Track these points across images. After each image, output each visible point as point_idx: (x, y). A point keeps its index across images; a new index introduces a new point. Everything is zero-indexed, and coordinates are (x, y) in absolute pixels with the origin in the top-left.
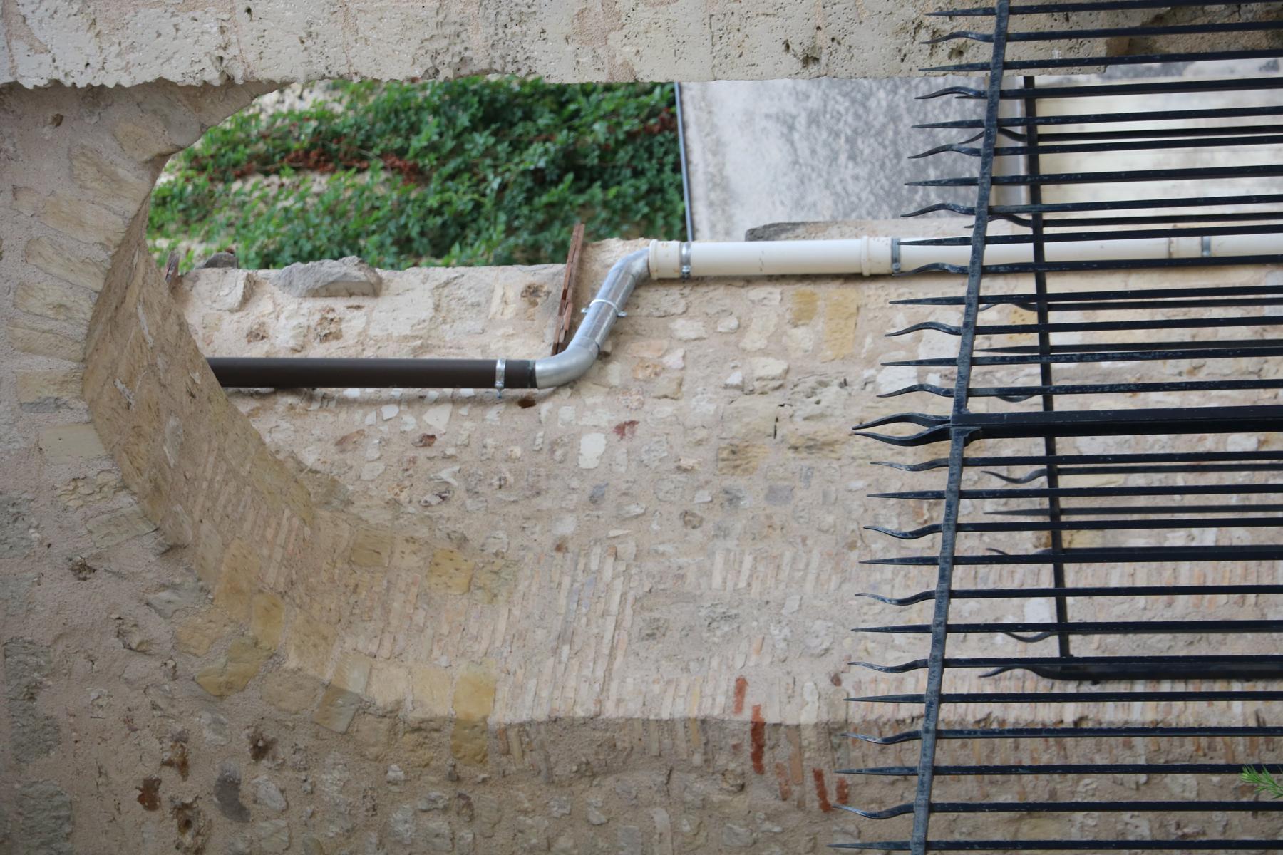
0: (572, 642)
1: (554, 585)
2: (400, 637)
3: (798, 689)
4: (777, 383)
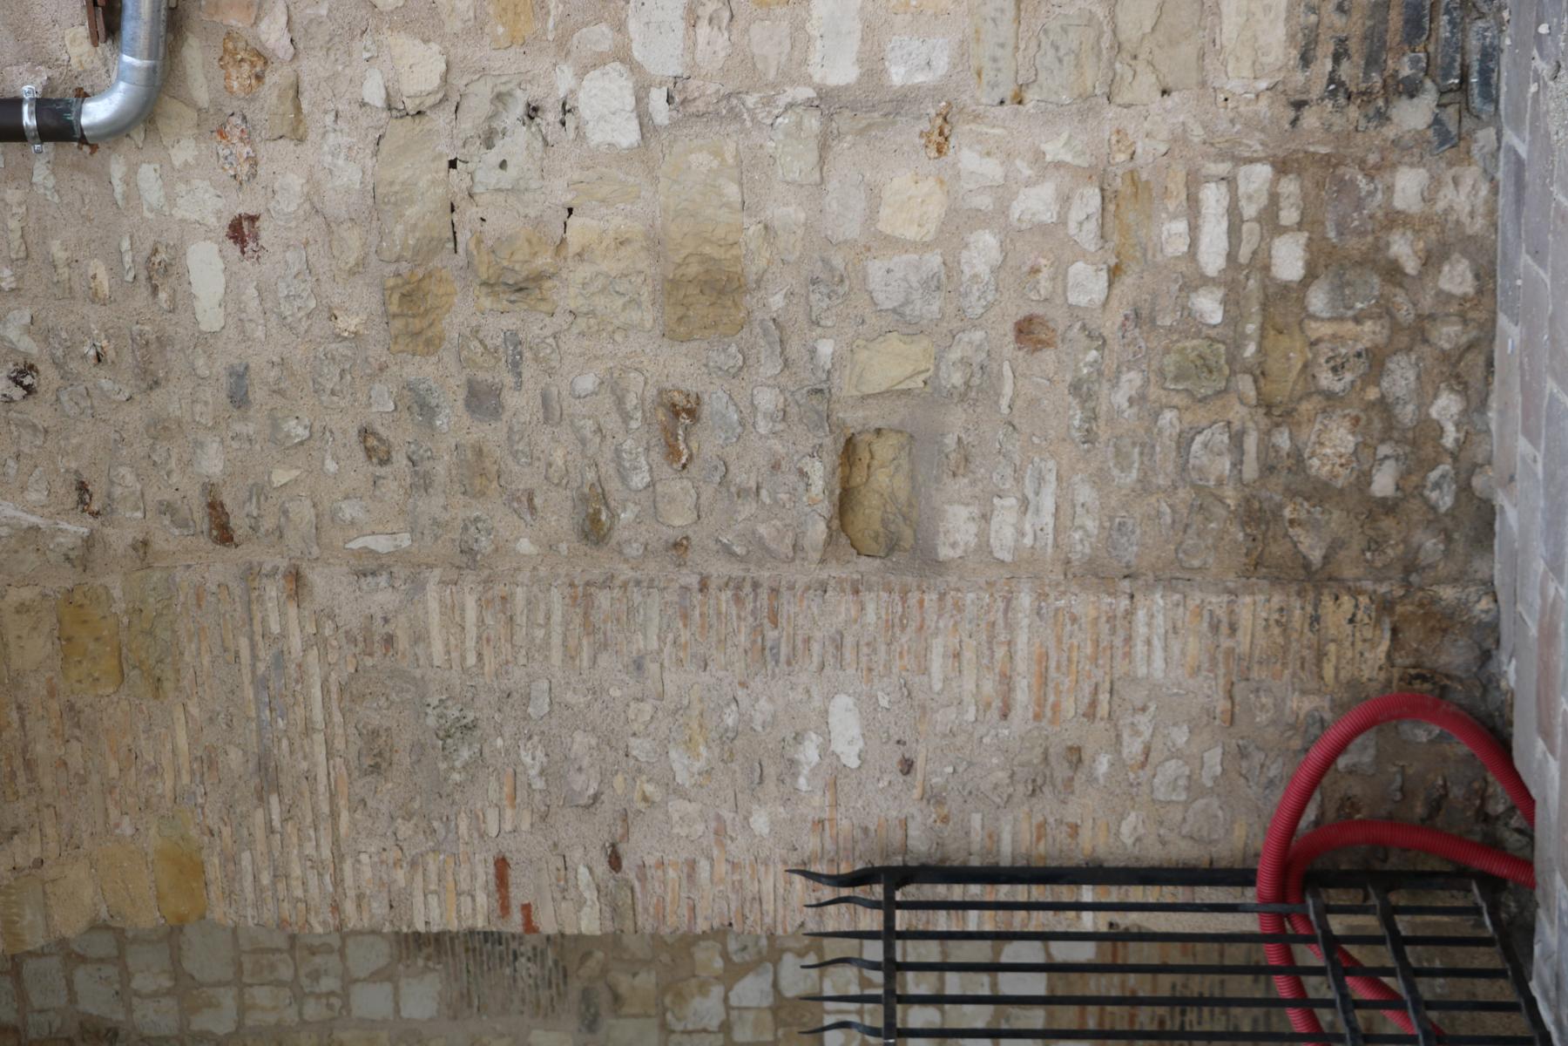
0: (278, 788)
1: (230, 657)
3: (571, 875)
4: (440, 96)
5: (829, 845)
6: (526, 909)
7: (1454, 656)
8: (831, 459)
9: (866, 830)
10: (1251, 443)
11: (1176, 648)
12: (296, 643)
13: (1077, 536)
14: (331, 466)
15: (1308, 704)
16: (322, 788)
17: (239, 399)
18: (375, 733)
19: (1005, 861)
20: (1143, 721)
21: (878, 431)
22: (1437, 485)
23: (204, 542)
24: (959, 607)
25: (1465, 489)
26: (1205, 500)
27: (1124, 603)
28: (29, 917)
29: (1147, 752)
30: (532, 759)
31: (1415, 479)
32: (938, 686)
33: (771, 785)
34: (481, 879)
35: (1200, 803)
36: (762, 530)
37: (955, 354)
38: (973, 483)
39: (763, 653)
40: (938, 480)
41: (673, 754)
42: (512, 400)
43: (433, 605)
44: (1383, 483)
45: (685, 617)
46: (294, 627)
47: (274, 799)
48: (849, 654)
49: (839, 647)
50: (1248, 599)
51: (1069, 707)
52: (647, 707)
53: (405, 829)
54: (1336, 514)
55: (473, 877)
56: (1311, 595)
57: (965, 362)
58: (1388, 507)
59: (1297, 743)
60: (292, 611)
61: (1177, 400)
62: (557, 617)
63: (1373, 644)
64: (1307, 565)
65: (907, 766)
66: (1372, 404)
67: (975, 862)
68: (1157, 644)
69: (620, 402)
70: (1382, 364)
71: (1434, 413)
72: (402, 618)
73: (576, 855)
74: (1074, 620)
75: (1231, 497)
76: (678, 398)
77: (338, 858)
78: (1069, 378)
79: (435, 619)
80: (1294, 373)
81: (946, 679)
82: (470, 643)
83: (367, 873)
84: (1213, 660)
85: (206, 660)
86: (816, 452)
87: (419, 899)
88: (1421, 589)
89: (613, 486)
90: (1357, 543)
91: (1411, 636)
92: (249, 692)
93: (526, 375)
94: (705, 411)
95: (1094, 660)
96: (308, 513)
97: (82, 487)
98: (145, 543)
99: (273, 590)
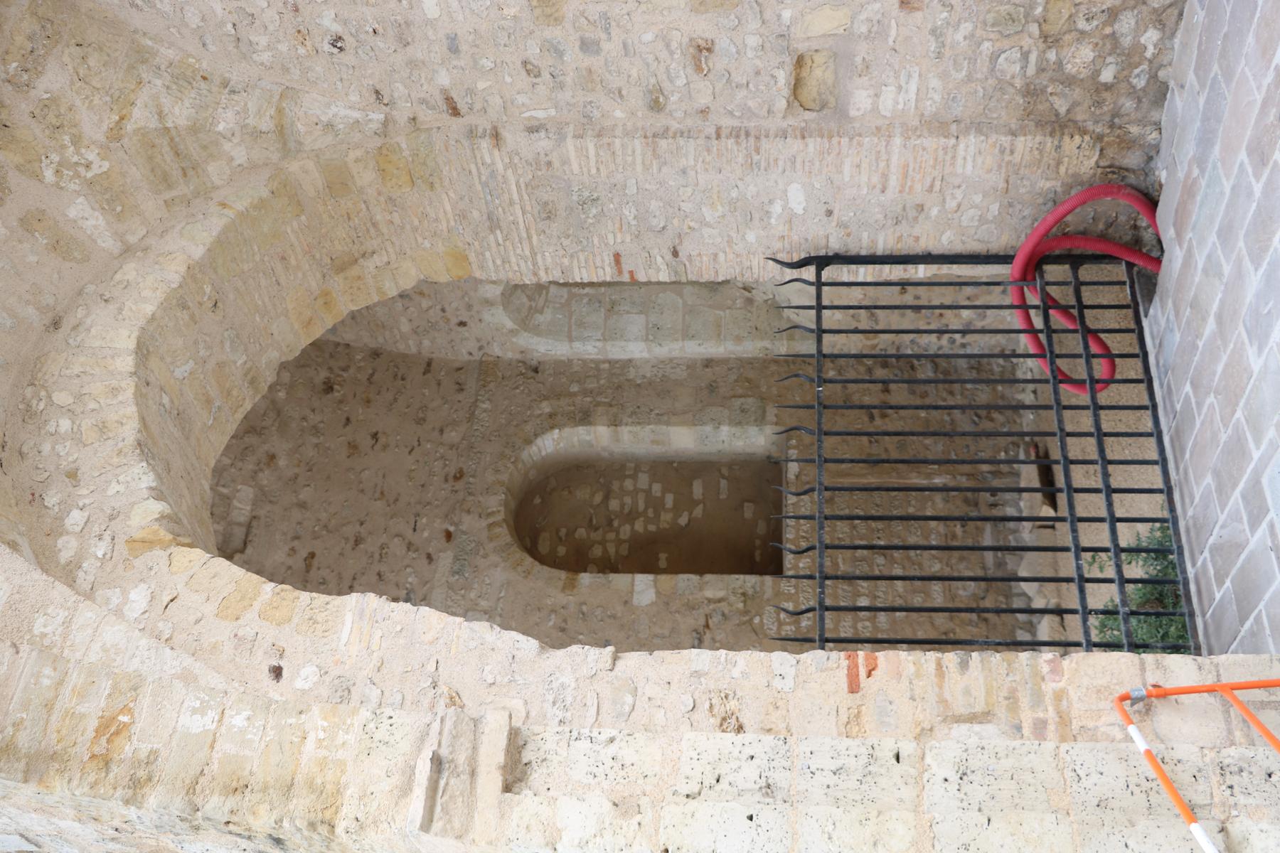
0: (500, 228)
2: (394, 239)
5: (787, 246)
6: (631, 273)
7: (1132, 159)
8: (789, 67)
9: (806, 240)
10: (1033, 58)
11: (979, 160)
12: (500, 166)
13: (929, 103)
14: (508, 79)
15: (1048, 185)
16: (522, 226)
17: (454, 49)
18: (546, 204)
19: (879, 253)
20: (959, 194)
21: (816, 51)
22: (1138, 76)
23: (446, 116)
24: (860, 144)
25: (1154, 77)
26: (1002, 85)
27: (953, 141)
28: (387, 284)
29: (959, 206)
30: (629, 213)
31: (1125, 73)
32: (847, 179)
33: (756, 222)
34: (607, 262)
35: (985, 227)
36: (750, 103)
37: (863, 16)
38: (870, 79)
39: (751, 165)
40: (850, 78)
41: (704, 209)
42: (605, 46)
43: (571, 148)
44: (1107, 76)
45: (708, 150)
46: (498, 159)
47: (498, 232)
48: (798, 165)
49: (794, 163)
50: (1022, 139)
51: (918, 187)
52: (689, 190)
53: (566, 242)
54: (1077, 90)
55: (603, 261)
56: (1057, 137)
57: (869, 20)
58: (1108, 87)
59: (1041, 200)
60: (496, 152)
61: (992, 36)
62: (638, 152)
63: (1089, 158)
64: (1057, 115)
65: (829, 213)
66: (1107, 36)
67: (863, 253)
68: (969, 159)
69: (668, 46)
70: (1116, 15)
71: (1143, 40)
72: (555, 154)
73: (655, 252)
74: (924, 149)
75: (1018, 83)
76: (701, 42)
77: (534, 254)
78: (929, 26)
79: (572, 154)
80: (1063, 21)
81: (851, 176)
82: (592, 163)
83: (549, 260)
84: (1000, 167)
85: (455, 174)
86: (781, 65)
87: (576, 270)
88: (1120, 128)
89: (666, 86)
90: (1088, 102)
91: (1110, 152)
92: (479, 187)
93: (613, 34)
94: (717, 48)
95: (934, 167)
96: (498, 101)
97: (377, 92)
98: (414, 119)
99: (485, 144)
